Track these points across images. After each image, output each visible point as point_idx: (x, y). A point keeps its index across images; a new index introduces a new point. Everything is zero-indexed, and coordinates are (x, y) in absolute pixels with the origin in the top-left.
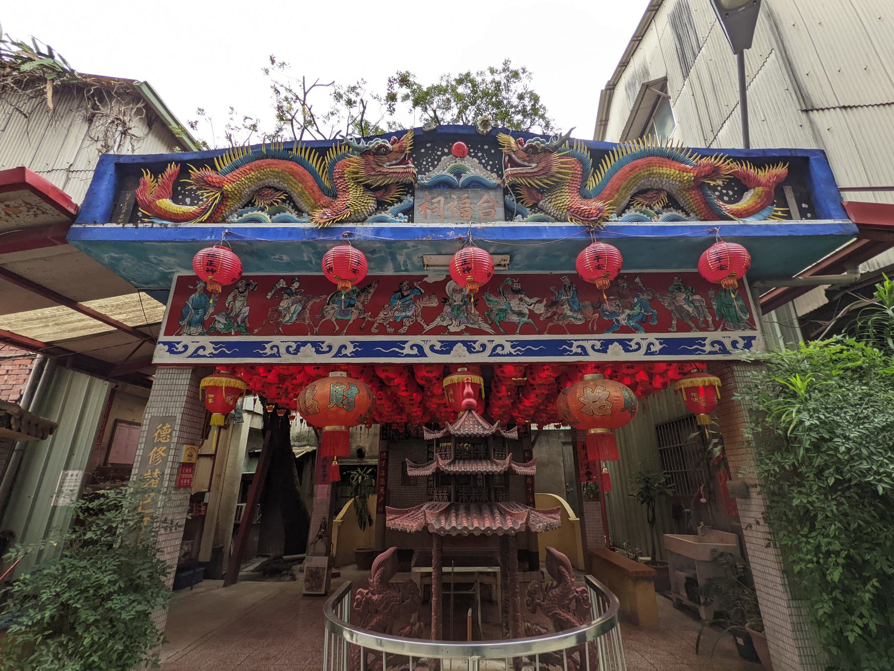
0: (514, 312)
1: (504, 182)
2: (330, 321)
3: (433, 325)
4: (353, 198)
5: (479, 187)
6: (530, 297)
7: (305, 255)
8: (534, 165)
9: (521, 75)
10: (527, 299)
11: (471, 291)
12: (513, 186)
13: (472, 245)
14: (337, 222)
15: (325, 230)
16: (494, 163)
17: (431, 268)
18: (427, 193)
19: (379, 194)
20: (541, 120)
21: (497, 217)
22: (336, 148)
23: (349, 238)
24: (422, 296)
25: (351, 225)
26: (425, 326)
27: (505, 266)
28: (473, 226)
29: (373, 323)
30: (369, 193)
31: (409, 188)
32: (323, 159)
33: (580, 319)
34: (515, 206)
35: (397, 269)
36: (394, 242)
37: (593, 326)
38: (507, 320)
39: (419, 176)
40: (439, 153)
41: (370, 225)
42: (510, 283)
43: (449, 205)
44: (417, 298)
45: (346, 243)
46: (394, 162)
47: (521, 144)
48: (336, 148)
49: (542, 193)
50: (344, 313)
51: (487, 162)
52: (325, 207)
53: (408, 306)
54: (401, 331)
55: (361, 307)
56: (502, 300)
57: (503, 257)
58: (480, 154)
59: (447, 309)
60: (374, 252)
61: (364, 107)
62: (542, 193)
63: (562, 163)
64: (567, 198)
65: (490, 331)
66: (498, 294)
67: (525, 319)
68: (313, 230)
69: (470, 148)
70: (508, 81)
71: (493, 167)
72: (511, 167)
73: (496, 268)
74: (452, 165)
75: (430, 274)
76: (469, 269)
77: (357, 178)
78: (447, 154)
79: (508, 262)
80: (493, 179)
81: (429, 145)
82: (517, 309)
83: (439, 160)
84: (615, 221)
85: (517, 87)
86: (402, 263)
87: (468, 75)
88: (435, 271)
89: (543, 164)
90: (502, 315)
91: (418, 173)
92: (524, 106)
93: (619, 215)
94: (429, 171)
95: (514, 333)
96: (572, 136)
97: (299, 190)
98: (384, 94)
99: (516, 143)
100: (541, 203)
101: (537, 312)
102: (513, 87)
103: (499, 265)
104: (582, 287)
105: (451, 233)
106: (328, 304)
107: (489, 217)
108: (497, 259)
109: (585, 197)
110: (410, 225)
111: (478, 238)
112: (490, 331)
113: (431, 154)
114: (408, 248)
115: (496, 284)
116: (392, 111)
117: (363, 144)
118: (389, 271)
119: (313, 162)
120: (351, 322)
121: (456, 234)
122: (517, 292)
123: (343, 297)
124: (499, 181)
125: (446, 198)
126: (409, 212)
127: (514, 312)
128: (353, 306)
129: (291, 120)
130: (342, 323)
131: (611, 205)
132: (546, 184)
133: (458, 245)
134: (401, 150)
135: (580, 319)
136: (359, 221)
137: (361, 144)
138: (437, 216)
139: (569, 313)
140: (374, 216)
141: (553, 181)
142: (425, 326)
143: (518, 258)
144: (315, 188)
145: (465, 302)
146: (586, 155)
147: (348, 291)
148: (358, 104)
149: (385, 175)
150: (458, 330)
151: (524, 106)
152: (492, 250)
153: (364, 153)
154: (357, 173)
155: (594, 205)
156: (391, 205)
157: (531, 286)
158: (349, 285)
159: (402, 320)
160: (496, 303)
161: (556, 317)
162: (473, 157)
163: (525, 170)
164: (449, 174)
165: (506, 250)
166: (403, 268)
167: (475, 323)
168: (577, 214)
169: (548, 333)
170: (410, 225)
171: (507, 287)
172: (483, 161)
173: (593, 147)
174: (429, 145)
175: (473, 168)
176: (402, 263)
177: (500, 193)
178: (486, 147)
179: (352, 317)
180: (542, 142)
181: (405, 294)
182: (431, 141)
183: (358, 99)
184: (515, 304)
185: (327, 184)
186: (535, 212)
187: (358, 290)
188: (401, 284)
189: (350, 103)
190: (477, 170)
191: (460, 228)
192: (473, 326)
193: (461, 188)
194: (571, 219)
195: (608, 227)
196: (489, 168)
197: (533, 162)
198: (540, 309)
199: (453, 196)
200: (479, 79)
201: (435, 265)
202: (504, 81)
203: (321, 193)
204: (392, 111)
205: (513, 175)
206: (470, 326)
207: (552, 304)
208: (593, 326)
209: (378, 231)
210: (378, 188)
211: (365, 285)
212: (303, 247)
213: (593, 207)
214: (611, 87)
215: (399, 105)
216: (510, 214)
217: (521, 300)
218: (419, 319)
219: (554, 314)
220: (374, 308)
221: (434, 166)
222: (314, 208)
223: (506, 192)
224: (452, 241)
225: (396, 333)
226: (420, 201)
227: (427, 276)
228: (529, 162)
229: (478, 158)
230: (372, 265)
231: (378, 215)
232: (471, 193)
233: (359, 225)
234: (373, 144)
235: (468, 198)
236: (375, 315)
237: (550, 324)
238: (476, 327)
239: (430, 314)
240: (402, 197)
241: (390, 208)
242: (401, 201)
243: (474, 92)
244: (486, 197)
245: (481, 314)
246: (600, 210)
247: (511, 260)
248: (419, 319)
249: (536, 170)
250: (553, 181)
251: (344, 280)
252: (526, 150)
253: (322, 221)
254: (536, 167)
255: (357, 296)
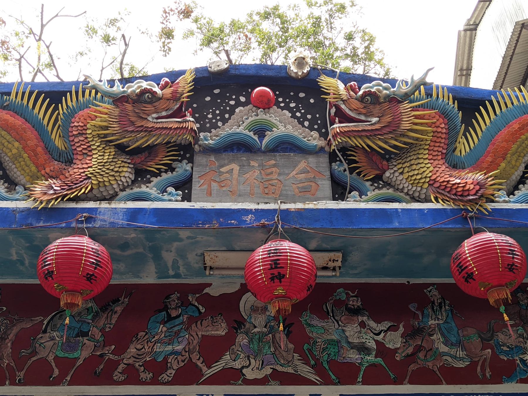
0: (352, 346)
1: (329, 144)
2: (44, 361)
3: (217, 367)
4: (96, 163)
5: (291, 150)
6: (378, 322)
7: (13, 251)
8: (375, 120)
9: (348, 9)
10: (372, 324)
11: (278, 312)
12: (344, 149)
13: (283, 238)
14: (70, 200)
15: (49, 213)
16: (314, 117)
17: (217, 272)
18: (212, 158)
19: (138, 159)
20: (378, 66)
21: (319, 194)
22: (77, 93)
23: (87, 225)
24: (201, 317)
25: (91, 205)
26: (204, 369)
27: (334, 269)
28: (284, 207)
29: (116, 364)
30: (123, 158)
31: (185, 151)
32: (56, 108)
33: (461, 359)
34: (349, 178)
35: (162, 274)
36: (158, 231)
37: (483, 370)
38: (340, 360)
39: (202, 135)
40: (232, 103)
41: (122, 205)
42: (344, 297)
43: (247, 175)
44: (192, 320)
45: (80, 232)
46: (164, 114)
47: (353, 90)
48: (77, 93)
49: (388, 160)
50: (70, 345)
51: (304, 116)
52: (52, 177)
53: (177, 333)
54: (164, 377)
55: (98, 336)
56: (331, 325)
57: (332, 255)
58: (292, 105)
59: (242, 339)
60: (125, 246)
61: (126, 45)
62: (388, 160)
63: (416, 117)
64: (429, 167)
65: (313, 377)
66: (324, 315)
67: (371, 358)
68: (28, 212)
69: (278, 96)
70: (330, 16)
71: (312, 122)
72: (340, 122)
73: (320, 273)
74: (251, 119)
75: (215, 281)
76: (281, 277)
77: (106, 136)
78: (244, 105)
79: (339, 264)
80: (314, 140)
81: (217, 91)
82: (356, 341)
83: (232, 112)
84: (505, 202)
85: (343, 24)
86: (170, 264)
87: (276, 8)
88: (223, 277)
89: (387, 119)
90: (333, 350)
91: (200, 130)
92: (354, 48)
93: (511, 193)
94: (216, 127)
95: (352, 381)
96: (428, 80)
97: (14, 151)
98: (159, 28)
99: (346, 89)
100: (387, 174)
101: (390, 346)
102: (337, 23)
103: (325, 268)
104: (463, 301)
105: (249, 218)
106: (45, 332)
107: (308, 195)
108: (322, 258)
109: (456, 166)
110: (186, 205)
111: (292, 226)
112: (313, 377)
113: (221, 104)
114: (181, 240)
115: (319, 298)
116: (166, 50)
117: (118, 88)
118: (149, 277)
119: (40, 112)
120: (80, 362)
121: (258, 219)
122: (355, 312)
123: (67, 321)
124: (322, 143)
125: (241, 166)
126: (184, 186)
127: (352, 346)
128: (85, 334)
129: (19, 60)
130: (65, 365)
131: (496, 177)
132: (395, 147)
133: (261, 235)
134: (175, 97)
135: (461, 359)
136: (105, 199)
137: (115, 88)
138: (229, 192)
139: (443, 348)
140: (128, 191)
141: (405, 143)
142: (204, 369)
143: (355, 257)
144: (39, 149)
145: (272, 328)
146: (453, 106)
147: (76, 310)
148: (117, 42)
149: (149, 131)
150: (260, 375)
151: (354, 48)
152: (313, 245)
153: (119, 100)
154: (106, 128)
155: (470, 178)
156: (156, 175)
157: (383, 302)
158: (79, 301)
159: (165, 359)
160: (322, 330)
161: (421, 355)
162: (282, 109)
163: (361, 126)
164: (247, 132)
165: (336, 244)
166: (171, 272)
167: (289, 363)
168: (444, 190)
169: (411, 383)
170: (186, 205)
171: (338, 303)
172: (298, 114)
173: (462, 95)
174: (217, 91)
175: (282, 123)
176: (170, 264)
177: (324, 160)
178: (302, 95)
179: (82, 354)
180: (386, 88)
181: (174, 314)
182: (219, 87)
183: (119, 35)
184: (352, 331)
185: (59, 143)
186: (378, 188)
187: (95, 308)
188: (168, 297)
189: (107, 39)
190: (289, 127)
191: (262, 210)
192: (285, 370)
193: (264, 152)
194: (436, 199)
195: (495, 210)
196: (306, 124)
197: (373, 116)
198: (394, 341)
199: (252, 163)
200: (290, 14)
201: (223, 270)
202: (325, 16)
203: (46, 157)
204: (166, 50)
205: (343, 134)
206: (279, 368)
207: (412, 333)
208: (483, 370)
209: (134, 214)
210: (138, 151)
211: (109, 298)
212: (11, 237)
213: (470, 181)
214: (472, 28)
215: (176, 43)
216: (340, 190)
217: (363, 325)
218: (195, 357)
219: (418, 349)
220: (120, 339)
221: (225, 121)
222: (34, 178)
223: (333, 157)
224: (251, 229)
225: (155, 382)
226: (201, 169)
227: (209, 285)
228: (365, 115)
229: (290, 110)
230: (122, 267)
231: (136, 190)
232: (279, 159)
233: (104, 205)
234: (134, 88)
235: (274, 166)
236: (121, 350)
237: (413, 367)
238: (290, 370)
239: (212, 349)
240: (174, 165)
241: (155, 180)
242: (173, 170)
243: (285, 30)
244: (302, 165)
245: (298, 350)
246: (481, 185)
247: (344, 260)
248: (195, 357)
249: (377, 126)
250: (405, 143)
251: (73, 291)
252: (362, 99)
253: (46, 198)
254: (378, 122)
255: (93, 319)
